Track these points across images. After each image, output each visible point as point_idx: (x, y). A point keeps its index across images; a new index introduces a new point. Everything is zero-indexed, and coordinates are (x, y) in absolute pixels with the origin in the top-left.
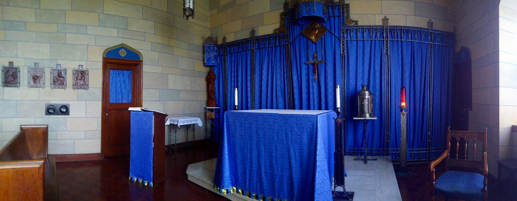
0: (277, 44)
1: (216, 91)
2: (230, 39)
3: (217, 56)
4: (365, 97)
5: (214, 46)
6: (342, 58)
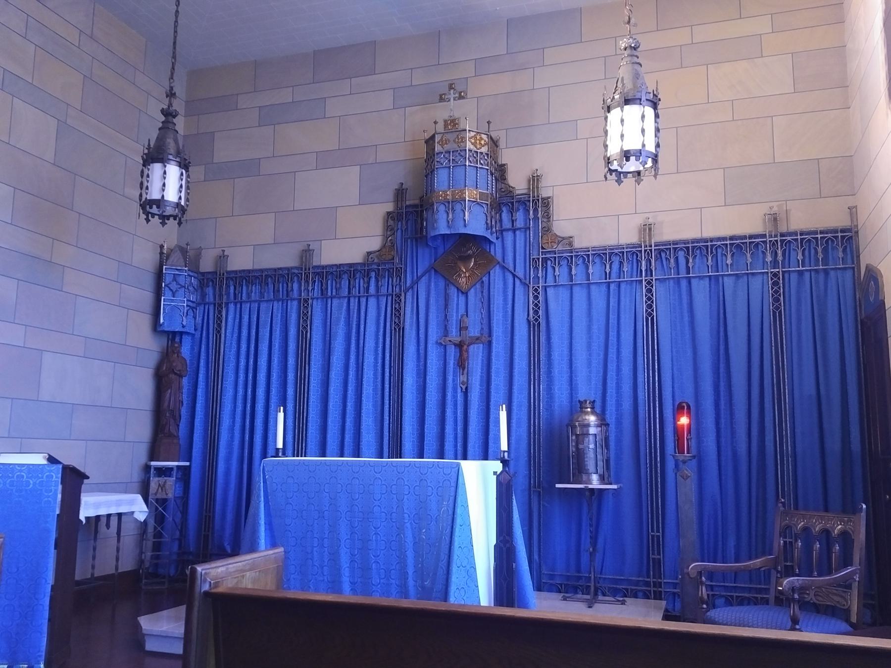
0: (372, 290)
1: (184, 411)
2: (240, 261)
3: (194, 305)
4: (588, 431)
5: (189, 275)
6: (532, 329)
